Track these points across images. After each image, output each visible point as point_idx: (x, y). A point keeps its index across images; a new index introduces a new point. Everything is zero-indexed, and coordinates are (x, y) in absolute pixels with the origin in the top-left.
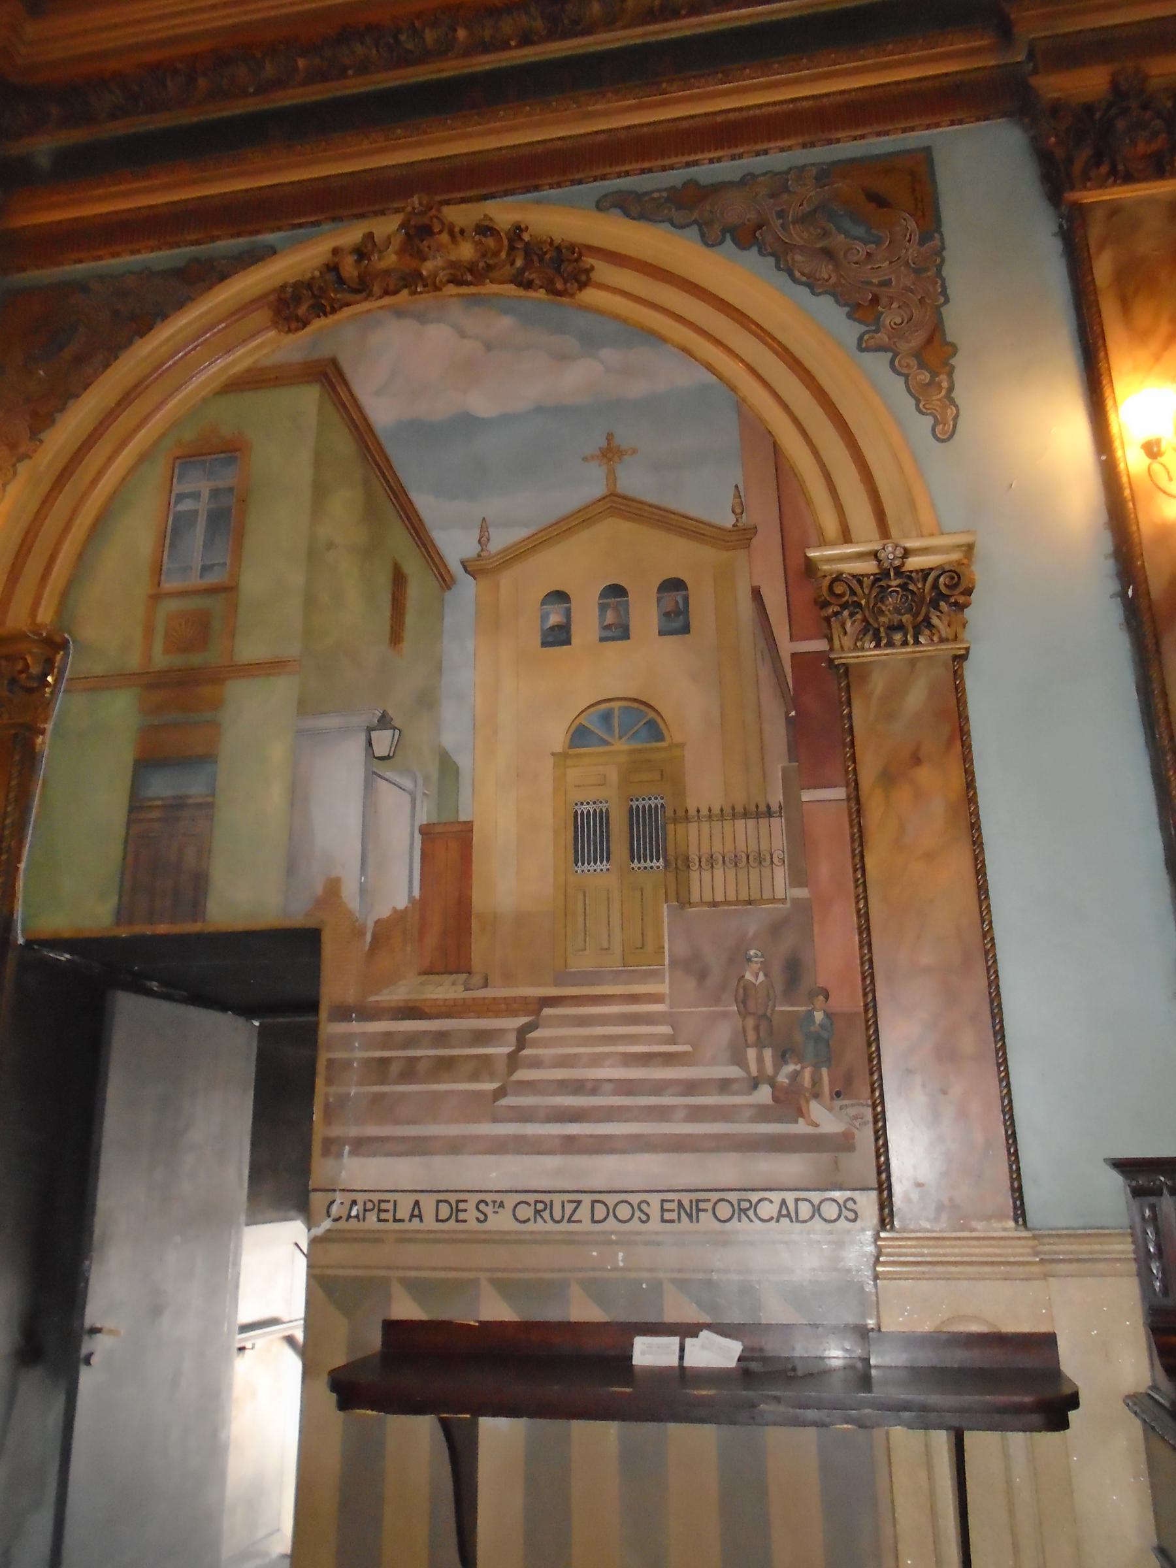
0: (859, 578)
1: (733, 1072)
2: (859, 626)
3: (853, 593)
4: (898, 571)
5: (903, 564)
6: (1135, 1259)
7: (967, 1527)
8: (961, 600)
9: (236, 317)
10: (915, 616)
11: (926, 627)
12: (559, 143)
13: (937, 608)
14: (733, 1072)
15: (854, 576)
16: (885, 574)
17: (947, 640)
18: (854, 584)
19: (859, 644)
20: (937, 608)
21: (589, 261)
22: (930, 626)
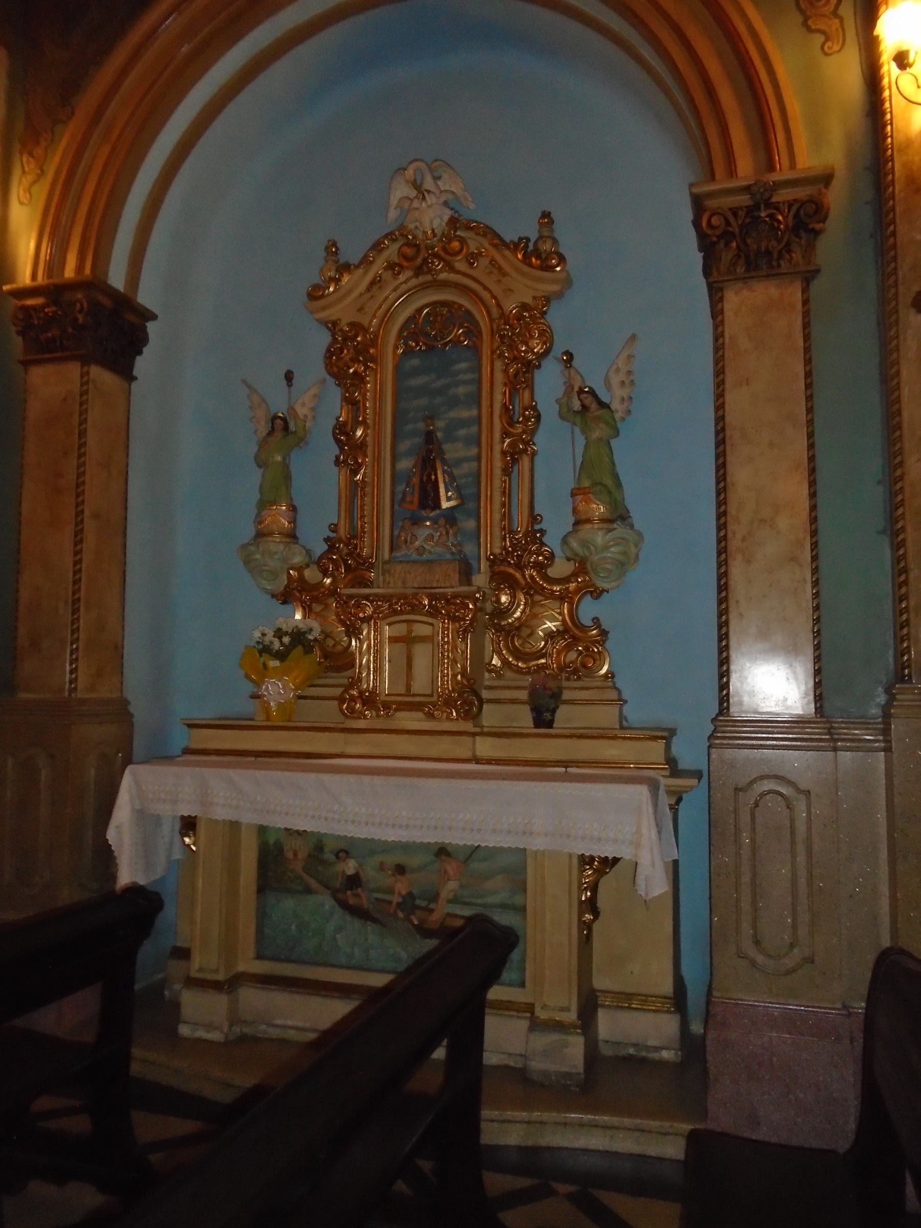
0: (734, 211)
3: (728, 223)
16: (756, 207)
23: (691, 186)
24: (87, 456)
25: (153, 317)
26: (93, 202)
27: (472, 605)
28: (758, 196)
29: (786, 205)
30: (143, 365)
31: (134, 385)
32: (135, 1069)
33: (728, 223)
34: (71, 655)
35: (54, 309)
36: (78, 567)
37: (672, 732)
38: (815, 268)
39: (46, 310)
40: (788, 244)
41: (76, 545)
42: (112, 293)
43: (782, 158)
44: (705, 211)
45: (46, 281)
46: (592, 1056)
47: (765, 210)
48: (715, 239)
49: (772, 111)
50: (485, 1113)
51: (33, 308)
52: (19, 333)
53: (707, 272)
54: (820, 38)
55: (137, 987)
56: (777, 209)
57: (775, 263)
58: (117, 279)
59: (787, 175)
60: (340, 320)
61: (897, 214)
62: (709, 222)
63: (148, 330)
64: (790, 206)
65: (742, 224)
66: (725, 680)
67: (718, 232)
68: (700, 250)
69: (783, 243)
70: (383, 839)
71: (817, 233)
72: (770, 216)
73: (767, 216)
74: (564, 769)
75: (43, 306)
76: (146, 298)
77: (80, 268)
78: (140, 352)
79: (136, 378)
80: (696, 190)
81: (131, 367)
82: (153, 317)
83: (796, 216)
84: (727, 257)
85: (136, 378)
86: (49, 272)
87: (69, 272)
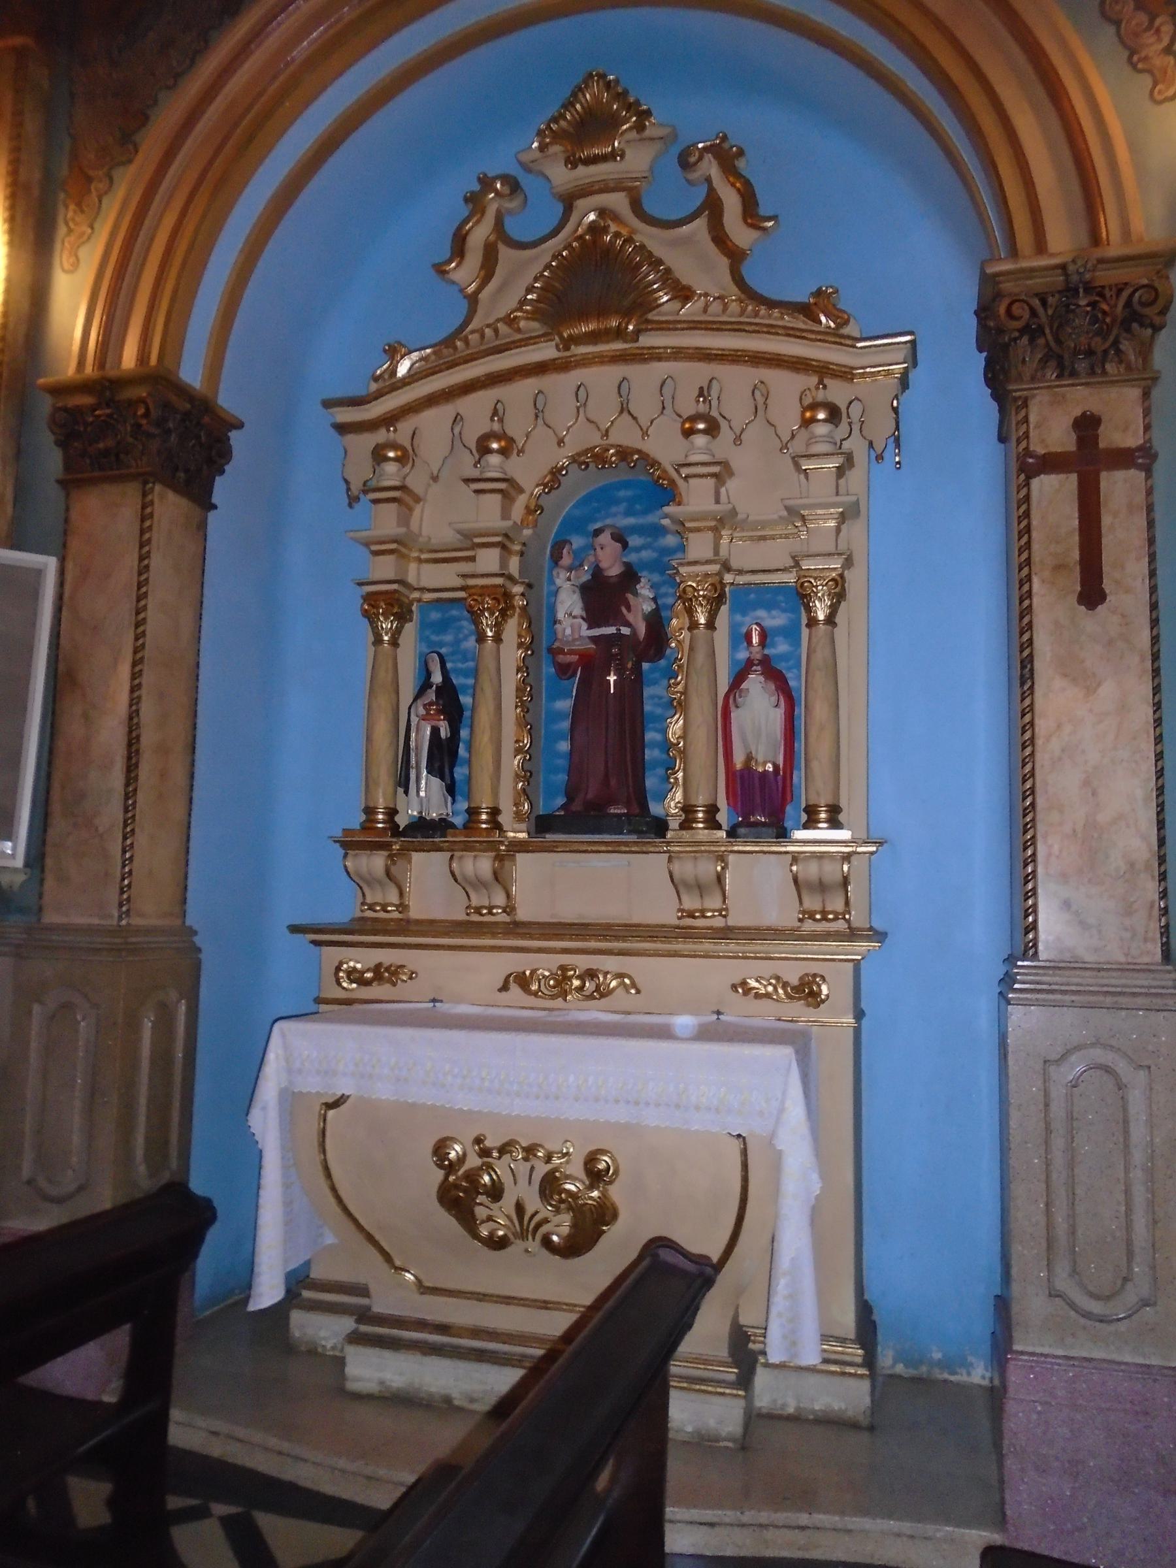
3: (1033, 313)
10: (1105, 339)
13: (1128, 330)
18: (1036, 302)
20: (1128, 330)
25: (239, 425)
29: (1114, 289)
30: (222, 489)
31: (212, 516)
33: (1033, 313)
35: (108, 411)
38: (1151, 375)
39: (97, 413)
40: (1116, 343)
42: (183, 390)
43: (1111, 226)
45: (97, 374)
48: (1016, 334)
52: (58, 443)
54: (1147, 80)
58: (192, 373)
59: (1113, 251)
60: (352, 580)
61: (1031, 426)
63: (232, 442)
64: (1120, 291)
65: (1052, 316)
66: (1031, 919)
70: (495, 1111)
71: (1157, 329)
72: (1093, 304)
73: (1088, 305)
74: (431, 1005)
76: (227, 401)
79: (215, 507)
80: (991, 270)
81: (209, 492)
82: (239, 425)
83: (1128, 304)
85: (215, 507)
86: (101, 362)
87: (129, 358)
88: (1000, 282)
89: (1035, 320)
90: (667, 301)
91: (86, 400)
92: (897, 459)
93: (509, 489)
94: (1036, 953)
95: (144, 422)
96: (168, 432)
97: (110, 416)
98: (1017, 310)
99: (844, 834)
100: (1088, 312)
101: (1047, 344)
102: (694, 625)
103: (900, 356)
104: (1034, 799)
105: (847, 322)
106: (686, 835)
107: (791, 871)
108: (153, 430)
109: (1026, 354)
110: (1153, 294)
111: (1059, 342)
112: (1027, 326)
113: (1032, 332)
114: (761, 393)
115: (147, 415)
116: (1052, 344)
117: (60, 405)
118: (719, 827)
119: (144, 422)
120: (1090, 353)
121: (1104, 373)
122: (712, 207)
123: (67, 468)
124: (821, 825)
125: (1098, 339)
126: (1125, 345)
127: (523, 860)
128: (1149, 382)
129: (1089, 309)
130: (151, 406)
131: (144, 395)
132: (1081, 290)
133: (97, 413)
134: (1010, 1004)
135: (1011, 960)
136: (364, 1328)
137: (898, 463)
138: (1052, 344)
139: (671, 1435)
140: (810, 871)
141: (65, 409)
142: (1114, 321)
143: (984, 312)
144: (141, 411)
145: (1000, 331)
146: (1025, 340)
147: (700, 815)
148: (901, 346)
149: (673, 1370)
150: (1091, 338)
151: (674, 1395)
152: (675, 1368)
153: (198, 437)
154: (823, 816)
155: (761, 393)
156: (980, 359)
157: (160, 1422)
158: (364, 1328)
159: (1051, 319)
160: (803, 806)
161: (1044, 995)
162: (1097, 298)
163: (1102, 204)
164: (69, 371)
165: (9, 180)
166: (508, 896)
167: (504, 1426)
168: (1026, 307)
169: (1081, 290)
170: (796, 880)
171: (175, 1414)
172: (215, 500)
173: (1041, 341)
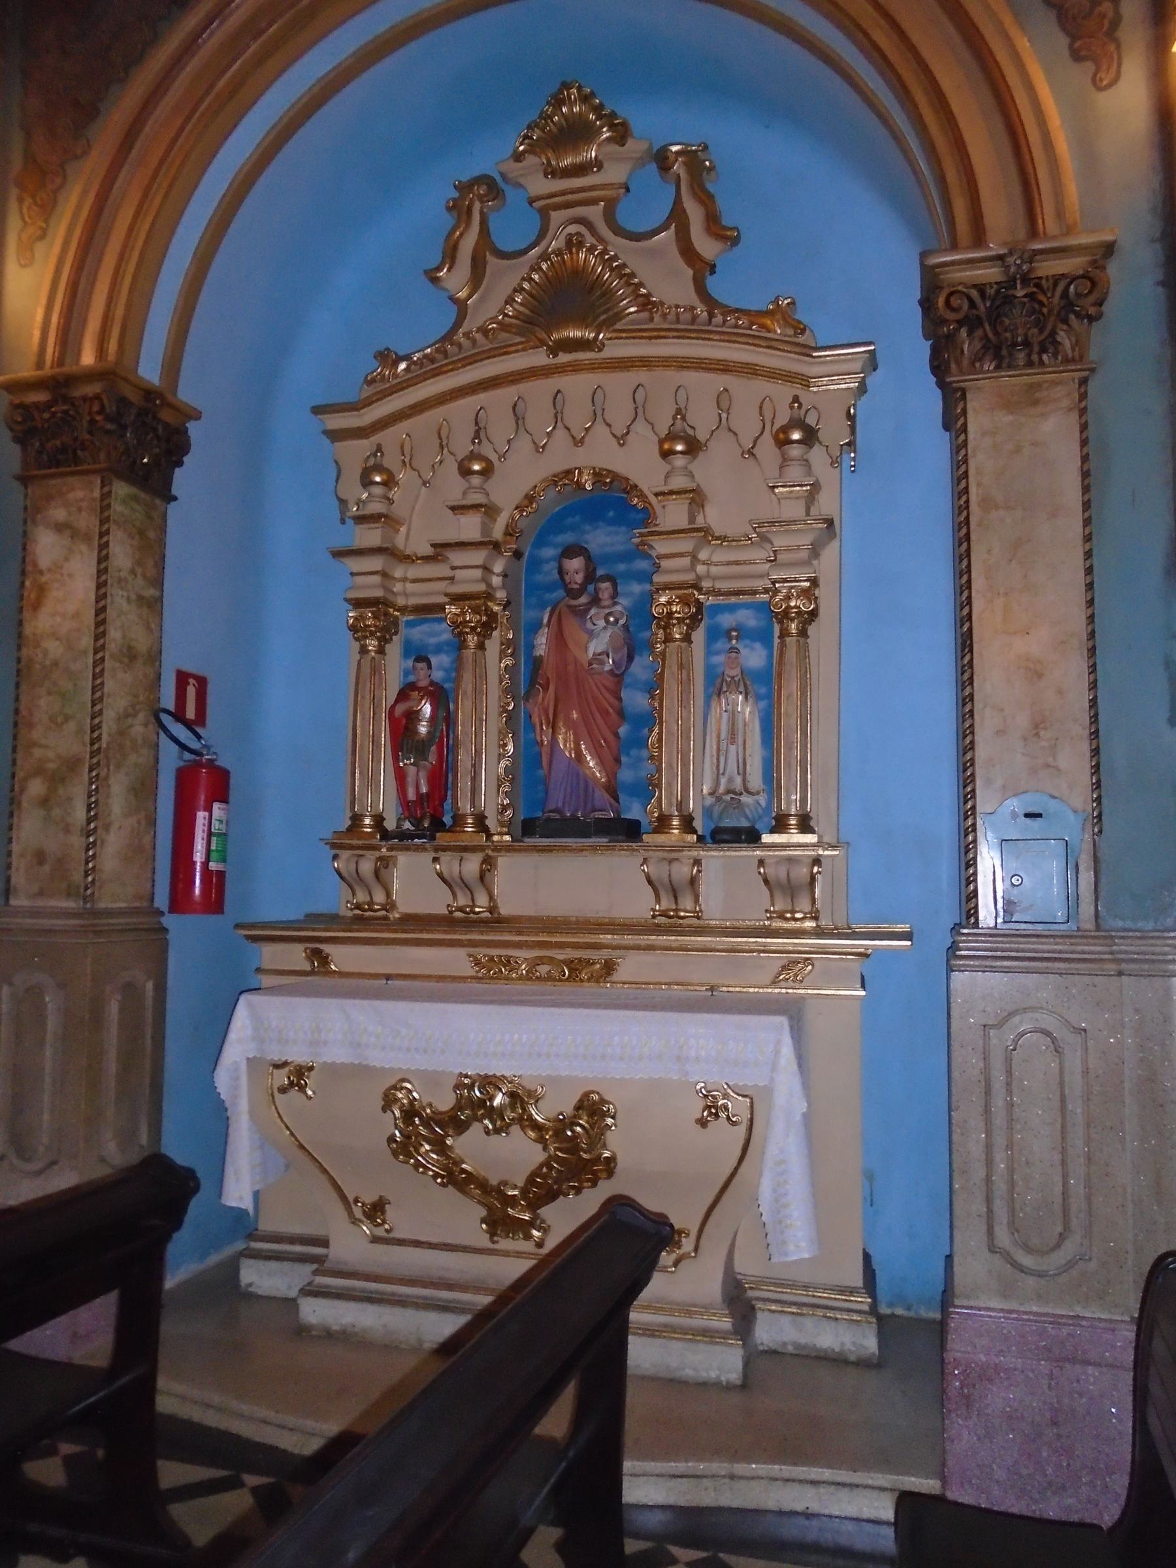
0: (981, 288)
1: (722, 789)
2: (978, 345)
3: (972, 304)
4: (1025, 280)
5: (1030, 270)
6: (41, 573)
7: (186, 331)
8: (1092, 311)
9: (741, 760)
10: (1041, 331)
11: (1050, 343)
12: (850, 1527)
13: (1065, 321)
14: (722, 789)
15: (975, 286)
16: (1011, 283)
17: (1073, 360)
18: (974, 293)
19: (977, 365)
20: (1065, 321)
21: (753, 1302)
22: (1056, 344)
23: (923, 255)
24: (109, 599)
25: (197, 416)
26: (122, 258)
27: (577, 713)
28: (1013, 269)
29: (1051, 281)
30: (182, 480)
32: (165, 1404)
33: (972, 304)
34: (91, 771)
36: (101, 629)
37: (426, 272)
40: (1053, 333)
41: (96, 639)
43: (1049, 221)
44: (941, 288)
46: (754, 1357)
47: (1022, 288)
49: (1034, 150)
50: (628, 1465)
51: (36, 405)
53: (939, 368)
55: (169, 1283)
56: (1038, 286)
57: (1035, 357)
62: (947, 303)
64: (1055, 285)
67: (960, 316)
68: (926, 337)
69: (1046, 333)
73: (1025, 296)
75: (48, 405)
76: (186, 394)
77: (101, 350)
78: (180, 464)
79: (175, 499)
82: (197, 416)
84: (967, 345)
85: (175, 499)
86: (60, 362)
88: (939, 274)
89: (974, 311)
90: (635, 312)
91: (41, 397)
92: (853, 463)
93: (489, 511)
94: (977, 919)
95: (98, 418)
96: (124, 427)
97: (66, 412)
98: (955, 301)
99: (811, 838)
100: (1025, 303)
101: (986, 335)
102: (668, 639)
103: (857, 366)
104: (974, 770)
105: (803, 331)
106: (660, 839)
107: (760, 873)
108: (109, 426)
109: (967, 345)
110: (1089, 284)
111: (996, 333)
112: (967, 317)
113: (972, 323)
114: (723, 401)
115: (102, 410)
116: (991, 335)
117: (17, 401)
118: (694, 831)
119: (98, 418)
120: (1027, 344)
121: (1041, 363)
122: (677, 216)
123: (25, 465)
124: (792, 831)
125: (1035, 331)
126: (1062, 336)
127: (502, 861)
128: (1086, 373)
129: (1026, 300)
130: (106, 402)
131: (98, 391)
132: (1018, 282)
133: (53, 409)
134: (953, 971)
135: (955, 929)
136: (321, 1280)
137: (854, 466)
138: (991, 335)
139: (630, 1372)
140: (776, 872)
141: (21, 406)
142: (1050, 311)
143: (926, 304)
144: (96, 408)
145: (944, 322)
146: (963, 333)
147: (470, 821)
148: (859, 356)
149: (634, 1316)
150: (1029, 329)
151: (630, 1338)
152: (635, 1316)
153: (155, 430)
154: (470, 821)
155: (723, 401)
156: (925, 347)
157: (147, 1388)
158: (321, 1280)
159: (989, 310)
160: (774, 814)
161: (986, 964)
162: (1035, 290)
163: (1041, 201)
164: (25, 371)
165: (581, 919)
166: (491, 897)
167: (453, 1359)
168: (965, 300)
169: (1018, 282)
170: (766, 881)
171: (162, 1382)
172: (175, 490)
173: (979, 333)
